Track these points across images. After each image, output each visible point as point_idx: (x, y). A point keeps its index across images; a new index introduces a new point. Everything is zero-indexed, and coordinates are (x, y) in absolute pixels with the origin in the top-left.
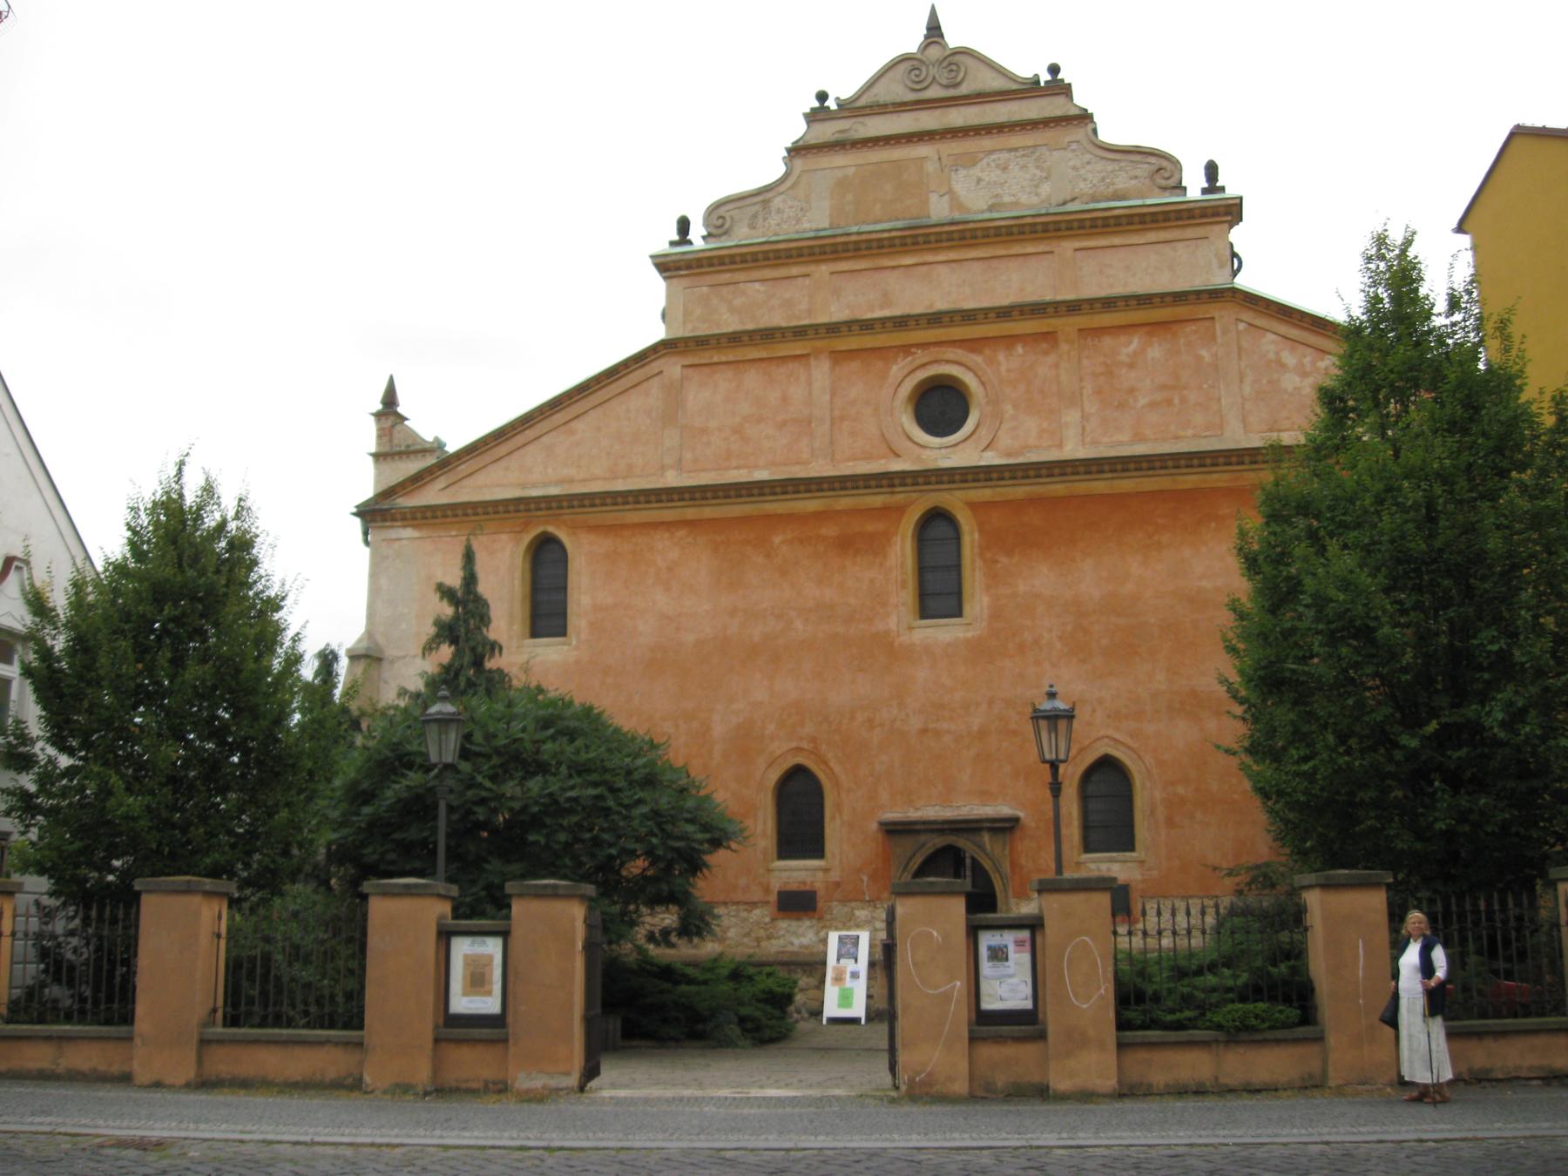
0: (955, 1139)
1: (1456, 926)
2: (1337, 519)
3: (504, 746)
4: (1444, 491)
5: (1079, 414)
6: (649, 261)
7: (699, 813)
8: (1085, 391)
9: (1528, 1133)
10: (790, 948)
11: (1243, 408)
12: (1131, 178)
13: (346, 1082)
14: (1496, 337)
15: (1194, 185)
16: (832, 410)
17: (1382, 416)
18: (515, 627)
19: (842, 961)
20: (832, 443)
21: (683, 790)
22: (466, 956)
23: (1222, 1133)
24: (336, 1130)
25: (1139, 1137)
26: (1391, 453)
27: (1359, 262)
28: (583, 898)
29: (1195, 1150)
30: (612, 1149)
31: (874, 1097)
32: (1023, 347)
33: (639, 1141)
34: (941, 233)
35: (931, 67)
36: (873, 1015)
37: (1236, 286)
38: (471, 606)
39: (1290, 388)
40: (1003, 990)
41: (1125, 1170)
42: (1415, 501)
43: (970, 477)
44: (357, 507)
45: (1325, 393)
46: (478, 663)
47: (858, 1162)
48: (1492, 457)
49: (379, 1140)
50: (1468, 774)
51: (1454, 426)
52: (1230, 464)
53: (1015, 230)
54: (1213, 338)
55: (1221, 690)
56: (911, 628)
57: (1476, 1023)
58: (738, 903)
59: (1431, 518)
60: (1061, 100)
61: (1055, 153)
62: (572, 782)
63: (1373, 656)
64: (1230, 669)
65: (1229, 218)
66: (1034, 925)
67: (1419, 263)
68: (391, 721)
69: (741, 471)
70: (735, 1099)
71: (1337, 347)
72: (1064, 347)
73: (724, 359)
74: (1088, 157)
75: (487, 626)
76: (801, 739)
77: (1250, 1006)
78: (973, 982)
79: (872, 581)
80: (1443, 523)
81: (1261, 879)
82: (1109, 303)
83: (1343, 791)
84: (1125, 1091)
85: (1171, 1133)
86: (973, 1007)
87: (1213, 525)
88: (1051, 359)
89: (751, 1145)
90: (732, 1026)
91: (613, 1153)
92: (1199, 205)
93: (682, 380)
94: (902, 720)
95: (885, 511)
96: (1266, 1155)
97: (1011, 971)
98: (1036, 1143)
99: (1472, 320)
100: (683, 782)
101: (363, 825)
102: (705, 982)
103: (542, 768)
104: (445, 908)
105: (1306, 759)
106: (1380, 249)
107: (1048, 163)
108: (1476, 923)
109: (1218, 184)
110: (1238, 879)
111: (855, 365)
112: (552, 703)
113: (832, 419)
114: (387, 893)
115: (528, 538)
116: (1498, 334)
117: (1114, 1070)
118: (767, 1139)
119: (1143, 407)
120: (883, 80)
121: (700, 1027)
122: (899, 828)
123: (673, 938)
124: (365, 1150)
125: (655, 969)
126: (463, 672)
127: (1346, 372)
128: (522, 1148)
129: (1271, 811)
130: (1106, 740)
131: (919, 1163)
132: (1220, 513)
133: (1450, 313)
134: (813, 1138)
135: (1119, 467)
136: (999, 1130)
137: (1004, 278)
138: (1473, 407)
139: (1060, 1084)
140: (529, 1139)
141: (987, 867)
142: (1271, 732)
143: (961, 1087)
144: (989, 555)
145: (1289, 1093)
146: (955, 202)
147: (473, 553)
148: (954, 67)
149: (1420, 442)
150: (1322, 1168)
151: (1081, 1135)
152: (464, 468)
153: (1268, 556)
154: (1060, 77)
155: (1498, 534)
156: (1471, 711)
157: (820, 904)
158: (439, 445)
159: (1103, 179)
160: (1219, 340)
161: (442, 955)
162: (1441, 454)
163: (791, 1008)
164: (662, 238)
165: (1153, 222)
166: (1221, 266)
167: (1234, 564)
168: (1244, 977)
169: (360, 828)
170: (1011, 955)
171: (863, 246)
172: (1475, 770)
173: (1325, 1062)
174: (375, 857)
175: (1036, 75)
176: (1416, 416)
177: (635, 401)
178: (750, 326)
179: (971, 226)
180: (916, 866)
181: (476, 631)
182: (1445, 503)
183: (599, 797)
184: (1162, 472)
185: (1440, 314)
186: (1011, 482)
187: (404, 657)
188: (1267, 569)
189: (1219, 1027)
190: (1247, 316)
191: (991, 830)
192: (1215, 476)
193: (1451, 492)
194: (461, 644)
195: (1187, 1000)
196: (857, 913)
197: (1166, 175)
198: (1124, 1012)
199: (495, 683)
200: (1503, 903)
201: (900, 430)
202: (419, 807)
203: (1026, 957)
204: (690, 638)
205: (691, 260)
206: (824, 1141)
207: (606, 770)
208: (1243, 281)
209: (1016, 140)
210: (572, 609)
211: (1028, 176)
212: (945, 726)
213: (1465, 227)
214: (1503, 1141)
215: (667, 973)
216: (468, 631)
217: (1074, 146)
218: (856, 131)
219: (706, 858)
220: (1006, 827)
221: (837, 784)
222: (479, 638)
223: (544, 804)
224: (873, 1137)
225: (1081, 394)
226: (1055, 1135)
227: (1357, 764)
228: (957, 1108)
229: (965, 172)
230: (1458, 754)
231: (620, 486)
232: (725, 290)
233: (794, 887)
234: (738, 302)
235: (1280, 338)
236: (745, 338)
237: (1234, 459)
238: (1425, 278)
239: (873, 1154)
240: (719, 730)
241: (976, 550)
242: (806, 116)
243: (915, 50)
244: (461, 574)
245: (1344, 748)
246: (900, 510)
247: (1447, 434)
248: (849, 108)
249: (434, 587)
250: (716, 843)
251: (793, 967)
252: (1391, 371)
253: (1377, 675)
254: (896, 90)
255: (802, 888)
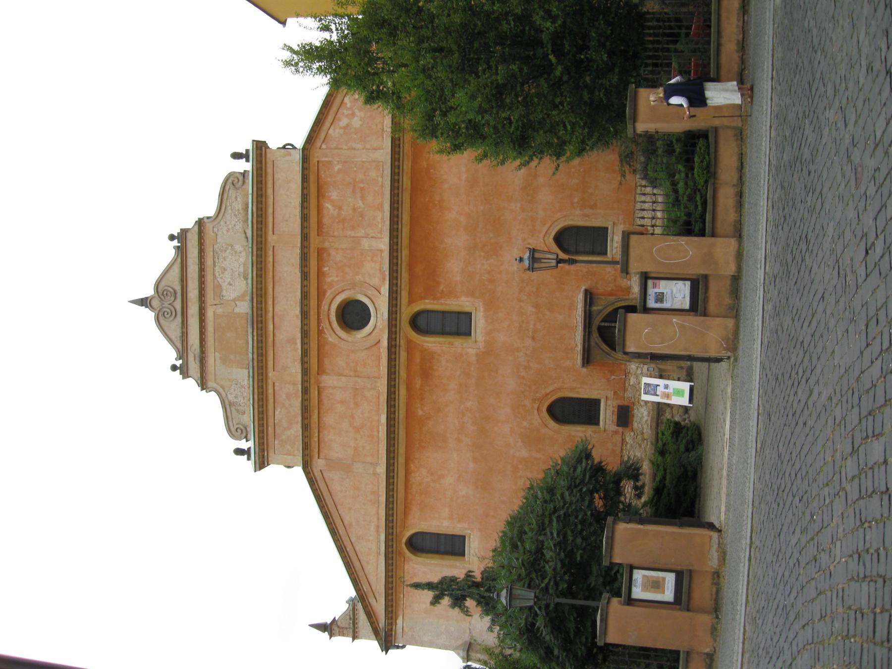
0: (758, 325)
1: (660, 54)
2: (437, 100)
3: (525, 570)
4: (427, 42)
5: (365, 240)
6: (258, 472)
7: (570, 464)
8: (352, 235)
9: (772, 23)
10: (649, 422)
11: (369, 149)
12: (237, 200)
13: (709, 663)
14: (347, 7)
15: (243, 166)
16: (350, 376)
17: (383, 72)
18: (458, 565)
19: (658, 393)
20: (369, 378)
21: (557, 472)
22: (643, 590)
23: (762, 182)
24: (734, 665)
25: (762, 226)
26: (403, 68)
27: (298, 76)
28: (614, 523)
29: (771, 196)
30: (753, 510)
31: (733, 370)
32: (325, 267)
33: (749, 496)
34: (257, 308)
35: (163, 305)
36: (689, 378)
37: (301, 147)
38: (445, 587)
39: (360, 123)
40: (679, 297)
41: (778, 232)
42: (431, 58)
43: (394, 302)
44: (382, 651)
45: (368, 101)
46: (477, 585)
47: (766, 375)
48: (410, 15)
49: (741, 640)
50: (580, 42)
51: (393, 34)
52: (399, 159)
53: (259, 266)
54: (329, 162)
55: (523, 171)
56: (476, 341)
57: (713, 46)
58: (622, 450)
59: (440, 50)
60: (189, 235)
61: (218, 241)
62: (549, 534)
63: (512, 86)
64: (513, 164)
65: (264, 148)
66: (645, 277)
67: (302, 44)
68: (507, 635)
69: (380, 430)
70: (730, 446)
71: (343, 90)
72: (327, 244)
73: (317, 435)
74: (222, 223)
75: (457, 578)
76: (533, 407)
77: (696, 164)
78: (674, 312)
79: (448, 361)
80: (444, 44)
81: (628, 159)
82: (305, 218)
83: (584, 108)
84: (738, 235)
85: (761, 209)
86: (688, 313)
87: (431, 171)
88: (333, 252)
89: (755, 434)
90: (690, 456)
91: (755, 509)
92: (255, 164)
93: (326, 459)
94: (526, 350)
95: (409, 351)
96: (775, 159)
97: (669, 291)
98: (762, 281)
99: (336, 20)
100: (553, 472)
101: (565, 654)
102: (665, 470)
103: (539, 551)
104: (615, 601)
105: (565, 126)
106: (292, 65)
107: (224, 245)
108: (658, 42)
109: (244, 153)
110: (627, 172)
111: (326, 361)
112: (503, 542)
113: (355, 376)
114: (605, 632)
115: (408, 554)
116: (345, 7)
117: (726, 240)
118: (752, 426)
119: (363, 204)
120: (168, 333)
121: (690, 474)
122: (586, 356)
123: (639, 484)
124: (746, 647)
125: (656, 497)
126: (482, 594)
127: (357, 88)
128: (750, 560)
129: (592, 148)
130: (546, 238)
131: (769, 342)
132: (425, 166)
133: (331, 31)
134: (753, 401)
135: (396, 219)
136: (754, 301)
137: (285, 275)
138: (383, 23)
139: (732, 269)
140: (745, 556)
141: (611, 309)
142: (549, 144)
143: (730, 323)
144: (438, 295)
145: (743, 147)
146: (241, 298)
147: (415, 583)
148: (165, 293)
149: (399, 52)
150: (783, 129)
151: (759, 257)
152: (366, 587)
153: (454, 138)
154: (176, 235)
155: (453, 16)
156: (545, 37)
157: (626, 403)
158: (351, 601)
159: (235, 215)
160: (330, 159)
161: (641, 604)
162: (406, 42)
163: (683, 423)
164: (245, 464)
165: (262, 190)
166: (290, 155)
167: (456, 158)
168: (680, 167)
169: (566, 656)
170: (661, 291)
171: (260, 351)
172: (577, 38)
173: (728, 127)
174: (583, 648)
175: (174, 248)
176: (387, 54)
177: (336, 487)
178: (300, 418)
179: (255, 290)
180: (608, 349)
181: (459, 585)
182: (434, 42)
183: (558, 518)
184: (400, 196)
185: (331, 36)
186: (399, 280)
187: (470, 629)
188: (461, 140)
189: (706, 182)
190: (318, 143)
191: (590, 306)
192: (405, 167)
193: (428, 38)
194: (466, 594)
195: (691, 199)
196: (632, 383)
197: (237, 181)
198: (695, 233)
199: (489, 577)
200: (650, 28)
201: (365, 339)
202: (556, 620)
203: (663, 283)
204: (471, 465)
205: (259, 449)
206: (755, 395)
207: (543, 514)
208: (299, 143)
209: (209, 262)
210: (450, 531)
211: (230, 257)
212: (531, 326)
213: (283, 20)
214: (775, 36)
215: (658, 491)
216: (458, 589)
217: (215, 230)
218: (195, 350)
219: (596, 462)
220: (590, 297)
221: (560, 389)
222: (463, 583)
223: (560, 550)
224: (754, 368)
225: (354, 237)
226: (759, 271)
227: (568, 99)
228: (742, 325)
229: (224, 291)
230: (566, 46)
231: (383, 499)
232: (278, 431)
233: (615, 417)
234: (285, 425)
235: (332, 127)
236: (306, 422)
237: (397, 156)
238: (310, 42)
239: (763, 367)
240: (524, 453)
241: (435, 302)
242: (184, 378)
243: (153, 314)
244: (426, 591)
245: (560, 106)
246: (409, 342)
247: (396, 38)
248: (182, 353)
249: (432, 607)
250: (588, 456)
251: (660, 421)
252: (359, 64)
253: (522, 85)
254: (175, 326)
255: (616, 413)
